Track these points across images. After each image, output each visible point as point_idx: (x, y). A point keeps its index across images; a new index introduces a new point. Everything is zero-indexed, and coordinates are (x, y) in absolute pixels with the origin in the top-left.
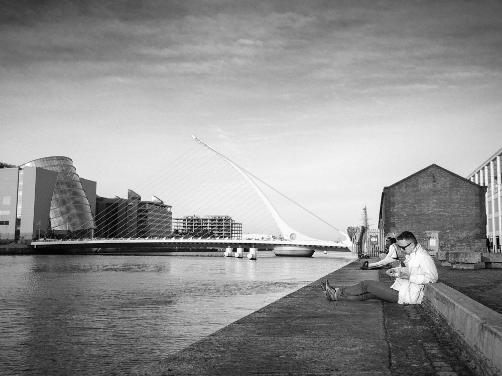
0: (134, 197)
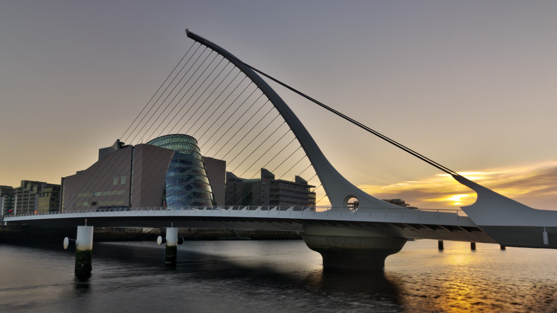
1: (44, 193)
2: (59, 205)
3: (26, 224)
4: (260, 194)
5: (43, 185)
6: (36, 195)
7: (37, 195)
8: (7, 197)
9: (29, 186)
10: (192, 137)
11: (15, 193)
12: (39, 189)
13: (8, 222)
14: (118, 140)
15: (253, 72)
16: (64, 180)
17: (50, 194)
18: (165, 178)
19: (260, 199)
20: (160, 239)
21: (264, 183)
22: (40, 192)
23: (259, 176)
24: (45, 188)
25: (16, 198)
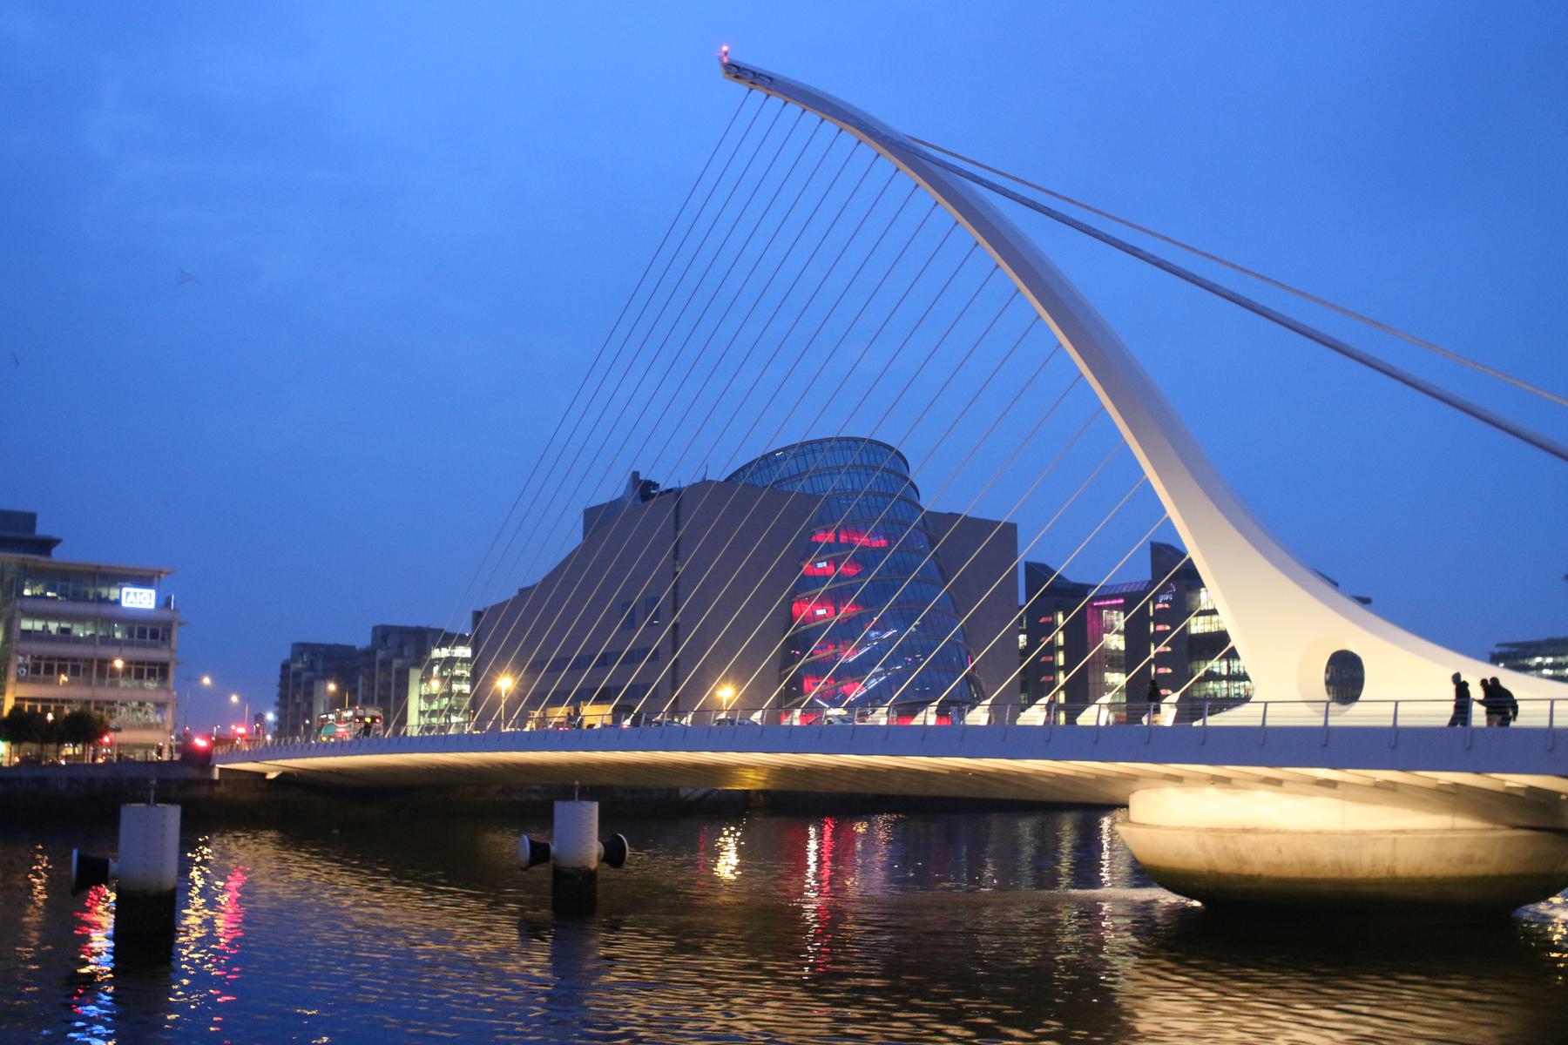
14: (636, 475)
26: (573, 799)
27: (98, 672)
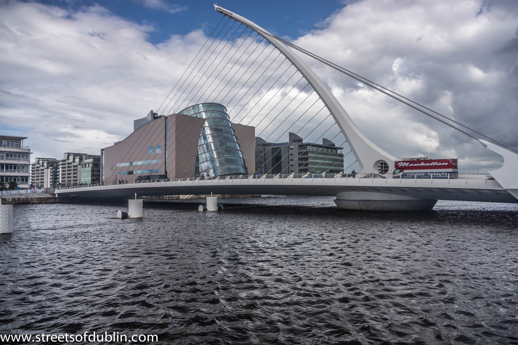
0: (294, 138)
1: (86, 164)
2: (100, 175)
3: (74, 195)
4: (289, 152)
5: (84, 156)
6: (78, 166)
7: (79, 167)
8: (52, 169)
9: (71, 158)
10: (220, 105)
11: (59, 165)
12: (81, 160)
13: (59, 194)
14: (152, 111)
15: (273, 39)
16: (103, 151)
17: (91, 165)
18: (197, 146)
19: (289, 168)
20: (201, 208)
21: (293, 147)
22: (82, 163)
23: (286, 139)
24: (86, 159)
25: (61, 169)
26: (134, 199)
27: (6, 169)
